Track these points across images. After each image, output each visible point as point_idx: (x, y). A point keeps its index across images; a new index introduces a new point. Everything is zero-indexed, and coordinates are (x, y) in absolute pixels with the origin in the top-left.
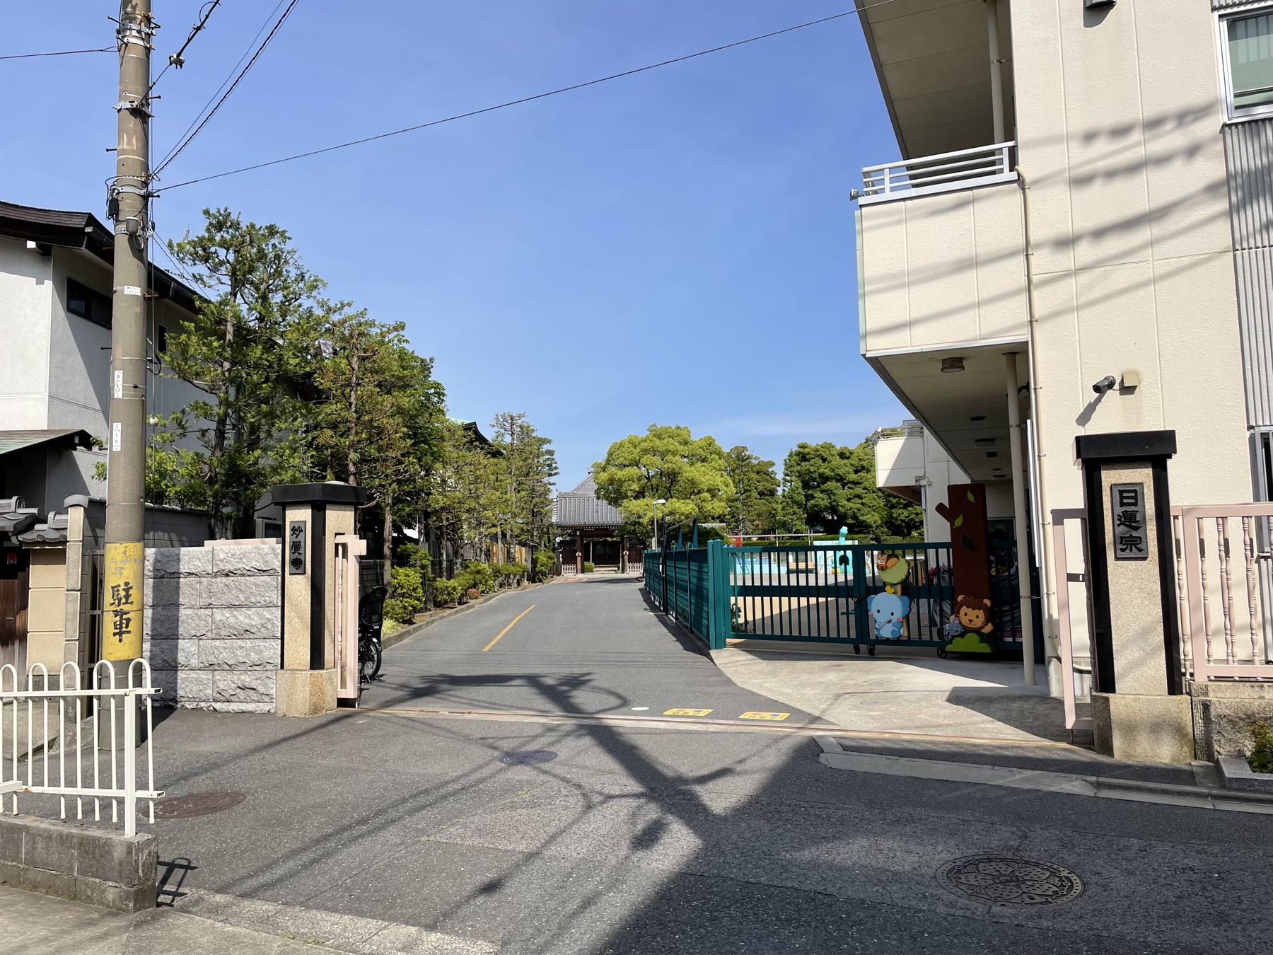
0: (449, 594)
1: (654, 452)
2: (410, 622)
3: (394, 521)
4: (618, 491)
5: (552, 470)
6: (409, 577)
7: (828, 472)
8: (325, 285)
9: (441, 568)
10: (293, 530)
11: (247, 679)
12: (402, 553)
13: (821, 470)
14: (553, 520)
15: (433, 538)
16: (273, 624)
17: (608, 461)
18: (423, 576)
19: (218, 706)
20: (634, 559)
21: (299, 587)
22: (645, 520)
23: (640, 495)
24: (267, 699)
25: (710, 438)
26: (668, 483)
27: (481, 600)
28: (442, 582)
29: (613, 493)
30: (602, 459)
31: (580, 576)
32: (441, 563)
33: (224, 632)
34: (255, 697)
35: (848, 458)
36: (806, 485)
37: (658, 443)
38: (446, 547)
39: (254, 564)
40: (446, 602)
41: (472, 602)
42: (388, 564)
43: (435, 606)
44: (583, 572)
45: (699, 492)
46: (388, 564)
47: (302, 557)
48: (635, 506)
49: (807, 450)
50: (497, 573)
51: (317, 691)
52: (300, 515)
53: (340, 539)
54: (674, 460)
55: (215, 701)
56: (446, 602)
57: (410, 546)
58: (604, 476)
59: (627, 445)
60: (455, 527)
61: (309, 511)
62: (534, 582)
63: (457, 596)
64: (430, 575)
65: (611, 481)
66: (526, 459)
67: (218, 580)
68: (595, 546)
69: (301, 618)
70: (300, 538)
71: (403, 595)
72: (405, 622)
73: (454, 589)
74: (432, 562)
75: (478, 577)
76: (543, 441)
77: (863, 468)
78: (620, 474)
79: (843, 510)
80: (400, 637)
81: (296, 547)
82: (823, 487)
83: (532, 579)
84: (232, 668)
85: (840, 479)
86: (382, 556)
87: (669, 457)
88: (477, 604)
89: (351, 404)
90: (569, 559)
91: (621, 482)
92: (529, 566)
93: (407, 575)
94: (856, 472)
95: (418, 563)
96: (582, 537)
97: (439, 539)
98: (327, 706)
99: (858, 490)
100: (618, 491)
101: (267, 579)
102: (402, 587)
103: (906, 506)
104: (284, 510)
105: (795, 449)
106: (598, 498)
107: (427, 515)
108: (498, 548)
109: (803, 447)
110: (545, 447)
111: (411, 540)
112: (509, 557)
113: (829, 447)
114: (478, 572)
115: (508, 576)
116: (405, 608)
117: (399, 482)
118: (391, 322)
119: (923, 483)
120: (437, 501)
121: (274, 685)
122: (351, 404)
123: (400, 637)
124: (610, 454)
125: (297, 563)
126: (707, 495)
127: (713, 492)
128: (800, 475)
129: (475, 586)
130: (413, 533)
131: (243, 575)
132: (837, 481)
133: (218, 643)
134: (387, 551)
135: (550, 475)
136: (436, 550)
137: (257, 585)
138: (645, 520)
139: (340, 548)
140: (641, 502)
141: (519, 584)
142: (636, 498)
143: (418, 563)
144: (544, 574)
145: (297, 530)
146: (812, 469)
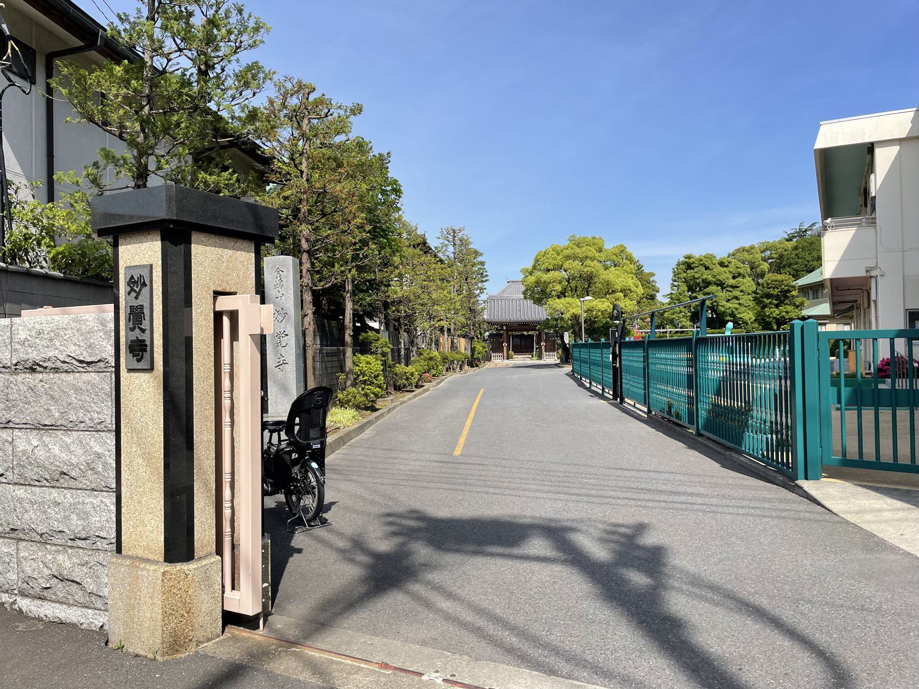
0: (407, 379)
1: (575, 258)
2: (374, 409)
3: (354, 310)
4: (543, 292)
5: (482, 276)
6: (370, 364)
7: (710, 278)
8: (268, 31)
9: (399, 355)
10: (131, 282)
11: (66, 562)
12: (363, 341)
13: (704, 277)
14: (485, 317)
15: (392, 329)
16: (105, 464)
17: (534, 267)
18: (384, 364)
19: (24, 604)
20: (551, 348)
21: (144, 393)
22: (567, 316)
23: (562, 295)
24: (99, 604)
25: (622, 246)
26: (584, 284)
27: (434, 383)
28: (401, 368)
29: (538, 294)
30: (529, 265)
31: (506, 361)
32: (399, 350)
33: (31, 474)
34: (79, 596)
35: (727, 266)
36: (691, 289)
37: (578, 250)
38: (404, 337)
39: (73, 350)
40: (405, 386)
41: (427, 385)
42: (349, 352)
43: (395, 389)
44: (508, 359)
45: (613, 292)
46: (349, 352)
47: (146, 337)
48: (559, 304)
49: (692, 260)
50: (445, 359)
51: (177, 608)
52: (142, 254)
53: (224, 304)
54: (592, 264)
55: (23, 594)
56: (405, 386)
57: (370, 333)
58: (532, 279)
59: (552, 252)
60: (411, 318)
61: (158, 244)
62: (472, 367)
63: (414, 381)
64: (390, 362)
65: (538, 283)
66: (467, 267)
67: (20, 378)
68: (518, 338)
69: (148, 457)
70: (143, 300)
71: (364, 382)
72: (367, 409)
73: (412, 374)
74: (392, 349)
75: (431, 363)
76: (477, 253)
77: (740, 274)
78: (545, 277)
79: (723, 309)
80: (362, 428)
81: (137, 315)
82: (706, 290)
83: (471, 365)
84: (44, 540)
85: (721, 284)
86: (343, 343)
87: (588, 262)
88: (431, 388)
89: (302, 172)
90: (497, 348)
91: (546, 284)
92: (469, 353)
93: (368, 363)
94: (734, 278)
95: (380, 351)
96: (507, 331)
97: (397, 329)
98: (200, 635)
99: (736, 293)
100: (543, 292)
101: (93, 377)
102: (364, 375)
103: (777, 306)
104: (116, 245)
105: (682, 259)
106: (525, 298)
107: (386, 305)
108: (445, 340)
109: (689, 257)
110: (480, 259)
111: (372, 329)
112: (453, 346)
113: (711, 257)
114: (431, 359)
115: (452, 362)
116: (366, 395)
117: (360, 269)
118: (349, 104)
119: (873, 273)
120: (396, 293)
121: (109, 578)
122: (302, 172)
123: (362, 428)
124: (537, 261)
125: (139, 349)
126: (621, 294)
127: (626, 292)
128: (686, 281)
129: (428, 371)
130: (375, 325)
131: (56, 370)
132: (718, 285)
133: (21, 492)
134: (348, 339)
135: (482, 281)
136: (395, 340)
137: (78, 390)
138: (567, 316)
139: (226, 321)
140: (563, 300)
141: (461, 369)
142: (559, 297)
143: (380, 351)
144: (478, 359)
145: (138, 283)
146: (696, 276)
